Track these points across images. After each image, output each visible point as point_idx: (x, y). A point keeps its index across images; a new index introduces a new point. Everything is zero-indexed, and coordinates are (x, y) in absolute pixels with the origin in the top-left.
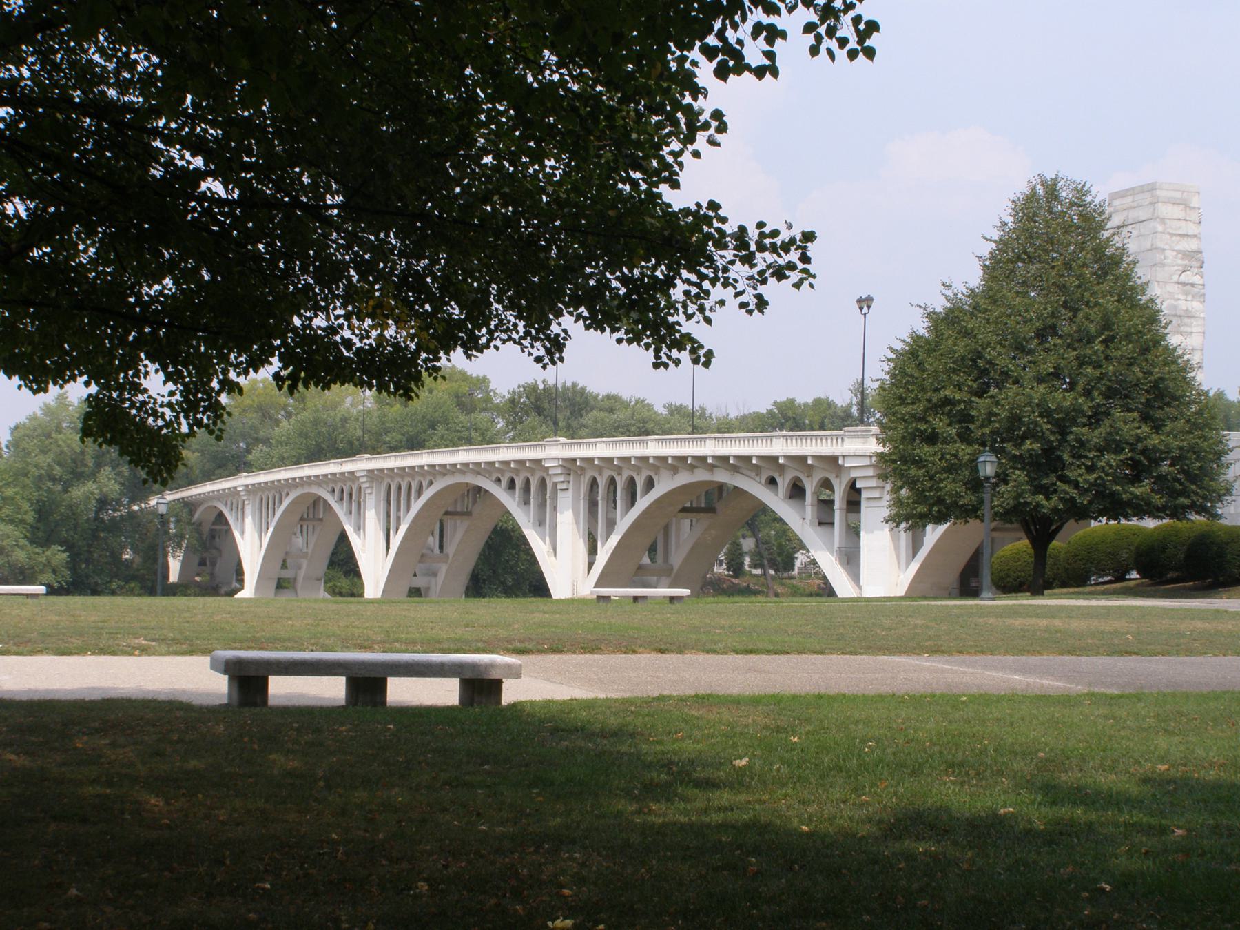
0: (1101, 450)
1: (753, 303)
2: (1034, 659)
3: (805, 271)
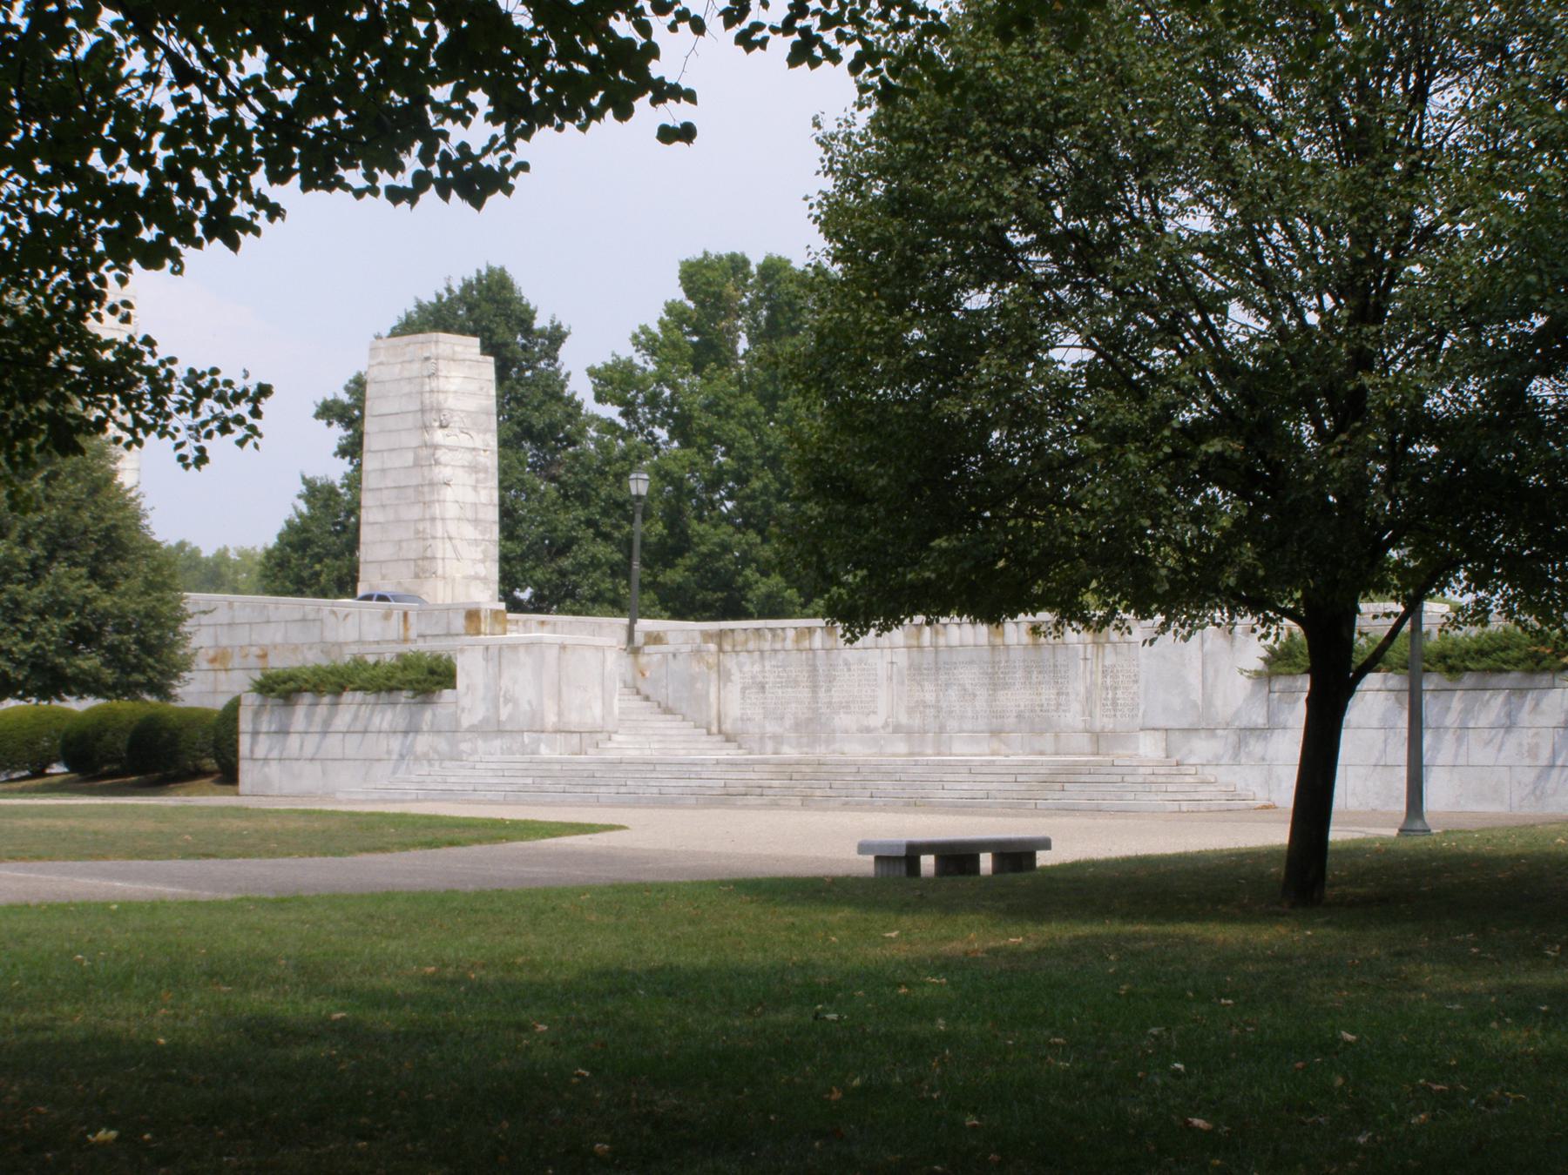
0: (41, 613)
1: (192, 454)
2: (104, 864)
3: (253, 429)
